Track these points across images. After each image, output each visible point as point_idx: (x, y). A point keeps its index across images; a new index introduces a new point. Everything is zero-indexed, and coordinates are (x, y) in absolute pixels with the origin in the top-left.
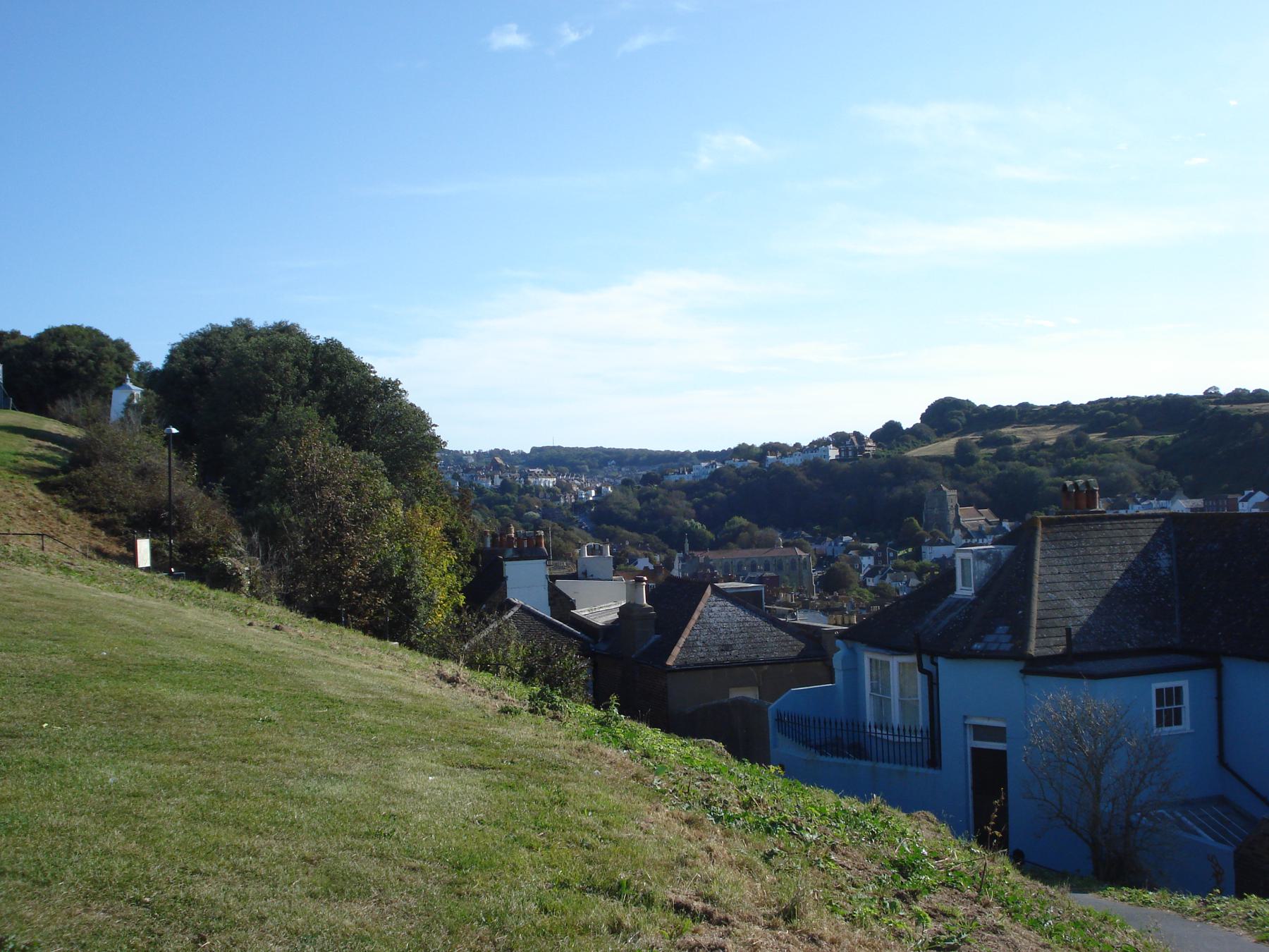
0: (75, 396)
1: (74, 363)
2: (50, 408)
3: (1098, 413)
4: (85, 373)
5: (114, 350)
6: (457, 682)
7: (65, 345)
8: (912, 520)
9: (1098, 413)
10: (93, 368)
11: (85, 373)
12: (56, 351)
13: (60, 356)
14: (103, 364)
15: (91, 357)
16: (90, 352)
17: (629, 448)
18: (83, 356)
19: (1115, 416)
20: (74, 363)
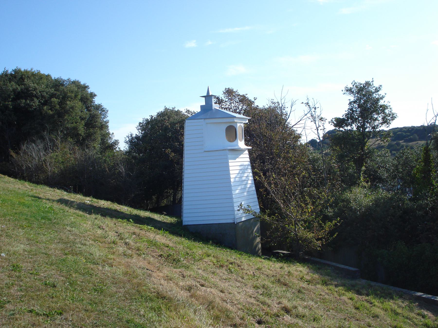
0: (42, 138)
1: (36, 102)
2: (12, 153)
3: (398, 133)
4: (51, 112)
5: (68, 80)
6: (137, 290)
7: (25, 85)
8: (256, 231)
9: (398, 133)
10: (58, 107)
11: (51, 112)
12: (14, 90)
13: (18, 95)
14: (68, 102)
15: (53, 96)
16: (52, 91)
17: (410, 125)
18: (45, 94)
19: (405, 134)
20: (36, 102)
